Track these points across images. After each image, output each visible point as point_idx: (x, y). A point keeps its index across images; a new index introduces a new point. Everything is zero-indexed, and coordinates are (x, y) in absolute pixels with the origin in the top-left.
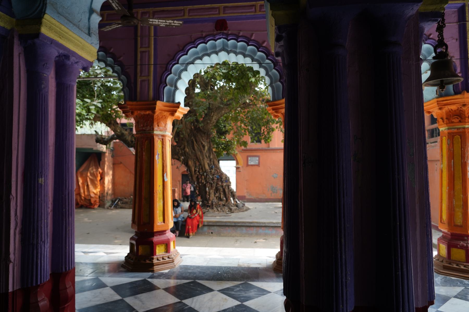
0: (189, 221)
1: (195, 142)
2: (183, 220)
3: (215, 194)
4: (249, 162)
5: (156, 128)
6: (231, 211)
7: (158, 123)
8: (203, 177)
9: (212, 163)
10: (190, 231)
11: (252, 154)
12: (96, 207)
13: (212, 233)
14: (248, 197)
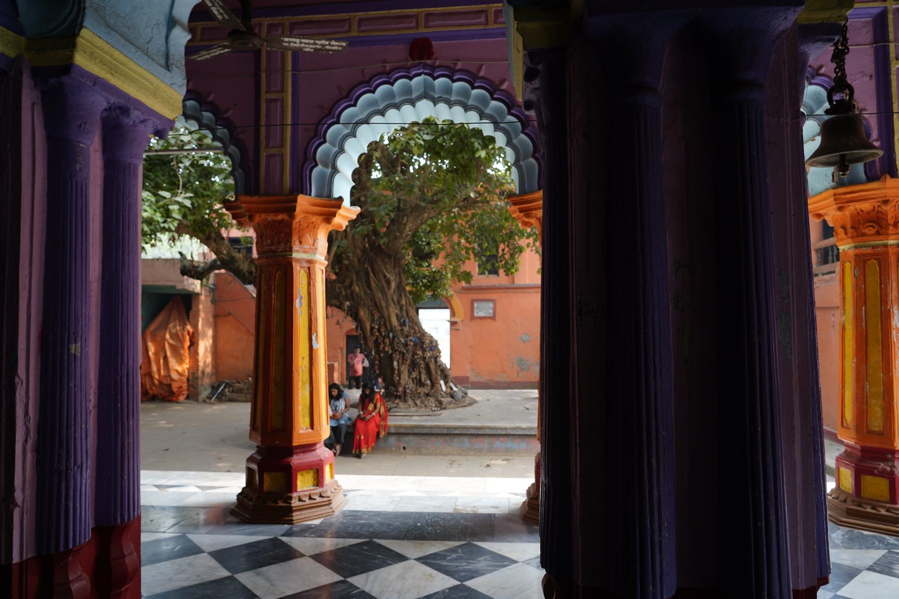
0: (360, 425)
1: (371, 275)
2: (349, 423)
3: (410, 373)
4: (475, 311)
6: (440, 405)
8: (387, 341)
9: (404, 313)
10: (363, 445)
12: (182, 398)
13: (404, 448)
14: (473, 379)
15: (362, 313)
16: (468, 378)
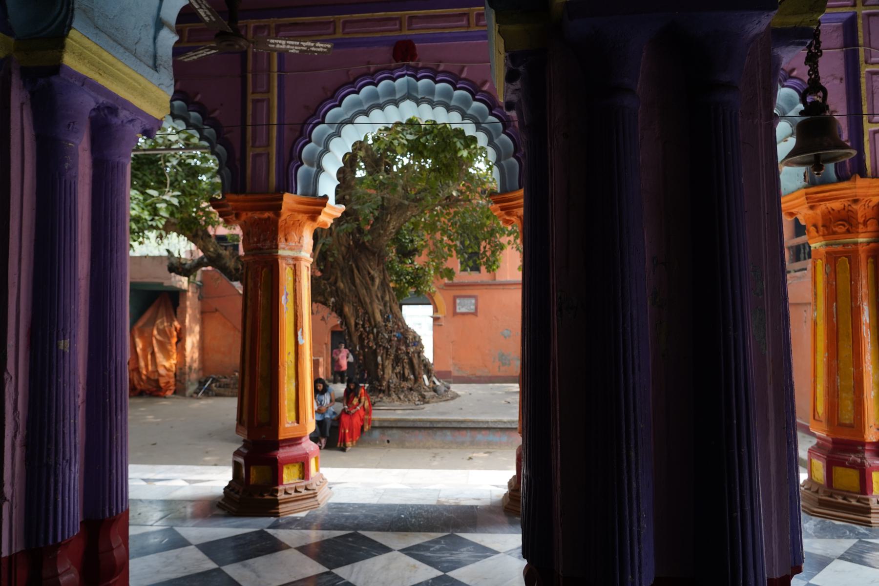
0: (345, 419)
1: (356, 271)
2: (334, 417)
3: (394, 368)
4: (458, 307)
5: (282, 244)
7: (285, 235)
9: (388, 309)
10: (347, 438)
11: (464, 293)
12: (169, 393)
13: (388, 441)
14: (455, 373)
16: (450, 372)
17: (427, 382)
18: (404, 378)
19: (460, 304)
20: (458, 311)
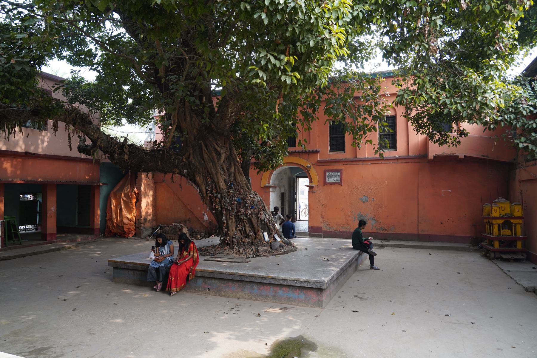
0: (173, 268)
1: (204, 148)
3: (237, 226)
4: (327, 179)
6: (257, 254)
8: (218, 201)
9: (232, 179)
10: (173, 284)
11: (331, 168)
12: (131, 235)
13: (209, 289)
14: (325, 229)
15: (198, 179)
16: (321, 227)
17: (267, 238)
18: (247, 236)
19: (329, 176)
20: (327, 181)
